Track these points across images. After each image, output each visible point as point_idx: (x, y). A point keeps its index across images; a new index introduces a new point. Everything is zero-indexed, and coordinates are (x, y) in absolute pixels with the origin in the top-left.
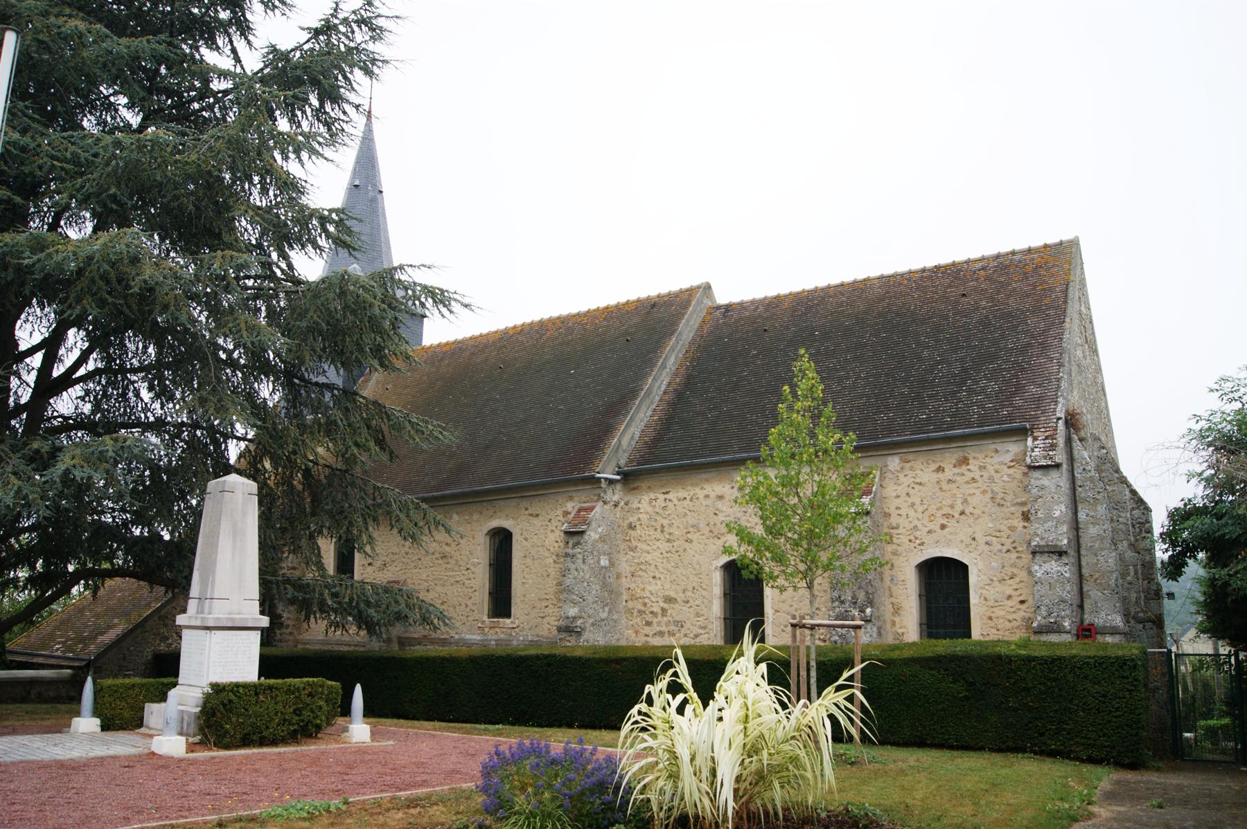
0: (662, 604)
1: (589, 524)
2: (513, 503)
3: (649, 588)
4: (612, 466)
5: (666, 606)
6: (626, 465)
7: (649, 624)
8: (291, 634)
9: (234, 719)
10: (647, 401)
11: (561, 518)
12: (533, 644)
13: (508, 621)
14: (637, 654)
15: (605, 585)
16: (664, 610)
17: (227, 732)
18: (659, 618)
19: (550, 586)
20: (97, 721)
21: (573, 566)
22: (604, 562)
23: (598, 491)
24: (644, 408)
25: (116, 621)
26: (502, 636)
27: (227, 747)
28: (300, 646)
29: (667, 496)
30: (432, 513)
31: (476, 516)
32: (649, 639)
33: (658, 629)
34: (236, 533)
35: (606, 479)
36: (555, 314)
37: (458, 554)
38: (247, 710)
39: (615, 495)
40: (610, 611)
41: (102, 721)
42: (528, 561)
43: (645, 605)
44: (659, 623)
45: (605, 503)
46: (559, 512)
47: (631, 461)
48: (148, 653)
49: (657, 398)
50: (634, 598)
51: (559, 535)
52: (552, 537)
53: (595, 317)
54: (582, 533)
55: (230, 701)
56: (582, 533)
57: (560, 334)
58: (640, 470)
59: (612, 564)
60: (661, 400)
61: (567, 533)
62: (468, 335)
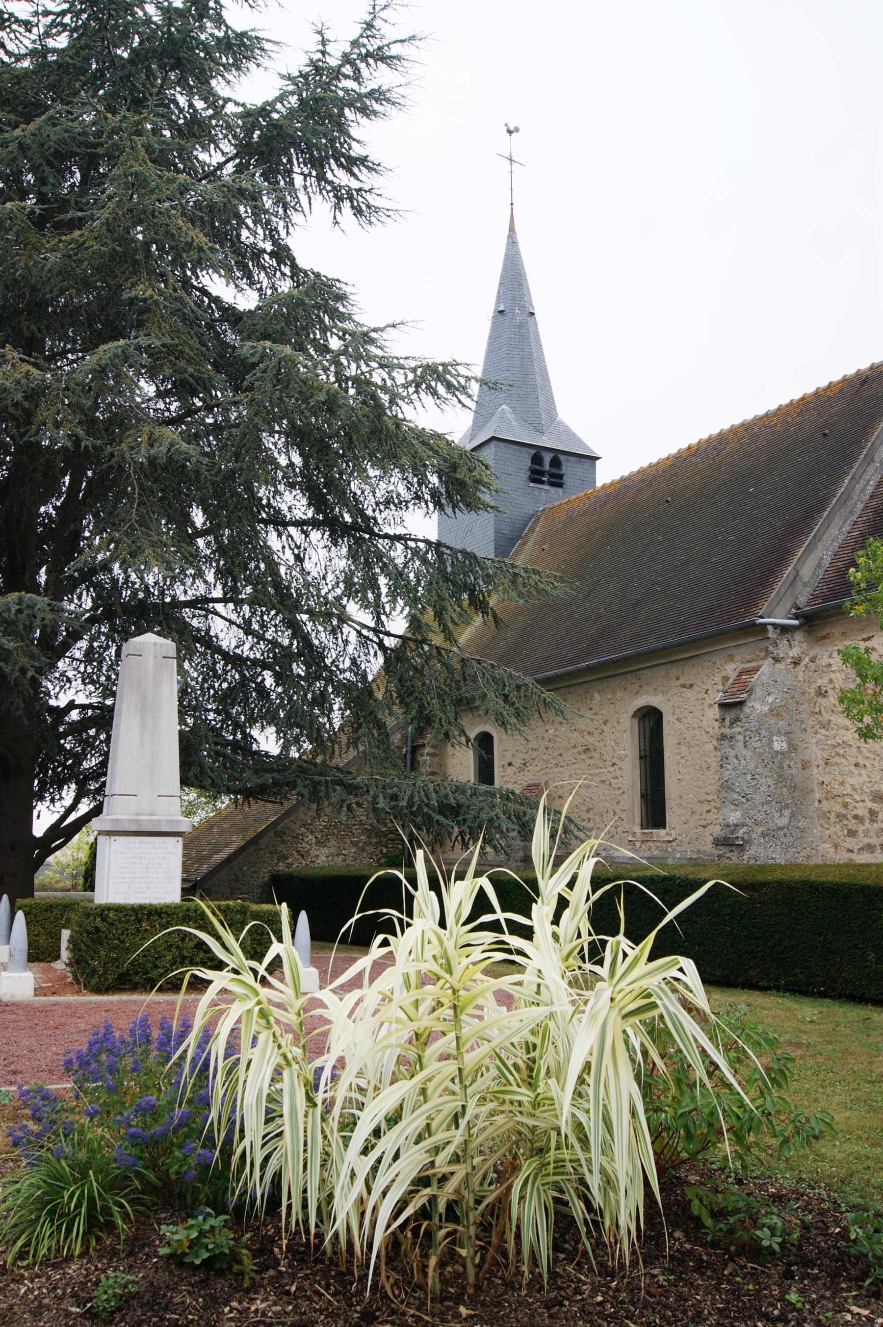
0: (870, 804)
1: (750, 692)
2: (661, 672)
3: (850, 780)
4: (787, 604)
5: (875, 807)
6: (808, 604)
7: (852, 833)
9: (103, 953)
10: (844, 512)
13: (662, 832)
14: (778, 876)
15: (781, 778)
16: (872, 812)
17: (94, 971)
18: (867, 825)
19: (711, 781)
21: (732, 753)
22: (779, 744)
23: (765, 644)
24: (837, 522)
27: (98, 991)
29: (869, 644)
30: (548, 695)
31: (619, 694)
32: (854, 856)
33: (866, 841)
34: (146, 708)
35: (775, 625)
37: (602, 744)
38: (123, 942)
39: (797, 646)
40: (793, 815)
43: (846, 805)
44: (867, 833)
45: (777, 660)
46: (718, 679)
47: (815, 597)
48: (264, 875)
49: (860, 506)
50: (830, 796)
51: (715, 712)
53: (787, 414)
54: (741, 704)
55: (97, 929)
56: (741, 704)
57: (742, 445)
58: (827, 610)
59: (793, 747)
60: (866, 508)
61: (724, 706)
62: (635, 469)
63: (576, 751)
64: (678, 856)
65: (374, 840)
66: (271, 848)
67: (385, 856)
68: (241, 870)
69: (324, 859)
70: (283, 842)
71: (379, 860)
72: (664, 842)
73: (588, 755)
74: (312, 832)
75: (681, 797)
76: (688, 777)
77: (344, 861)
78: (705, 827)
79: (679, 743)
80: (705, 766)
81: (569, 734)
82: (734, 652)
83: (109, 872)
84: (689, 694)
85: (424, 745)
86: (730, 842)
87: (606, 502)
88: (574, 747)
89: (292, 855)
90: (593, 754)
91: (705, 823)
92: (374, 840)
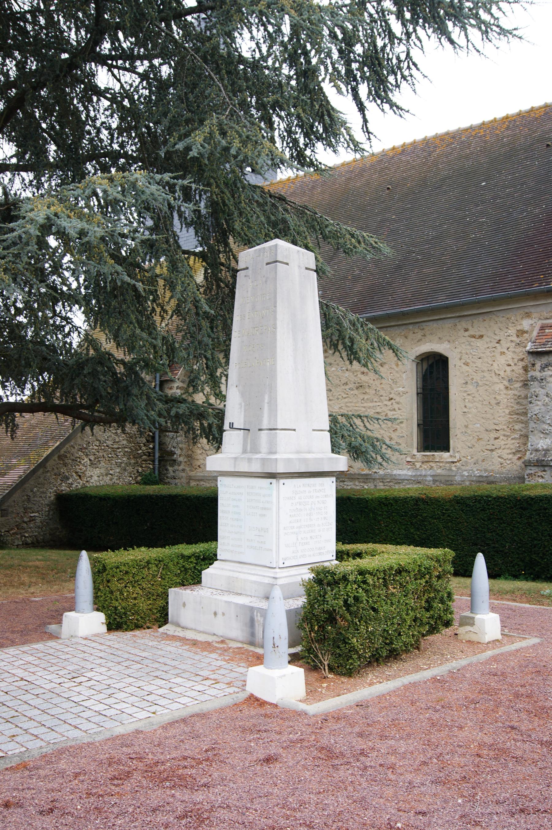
2: (448, 324)
8: (183, 470)
11: (514, 338)
12: (480, 480)
13: (445, 455)
20: (101, 617)
25: (14, 461)
26: (439, 471)
28: (193, 484)
36: (441, 130)
41: (108, 617)
42: (471, 388)
46: (512, 331)
52: (502, 360)
57: (454, 149)
63: (347, 387)
64: (466, 473)
65: (133, 461)
66: (56, 471)
67: (140, 474)
68: (32, 491)
69: (96, 478)
70: (65, 465)
71: (136, 477)
72: (447, 462)
73: (361, 390)
74: (87, 455)
75: (466, 427)
76: (474, 411)
77: (111, 480)
78: (492, 450)
79: (466, 383)
80: (493, 402)
81: (340, 373)
82: (532, 310)
83: (278, 523)
84: (479, 343)
85: (172, 381)
86: (544, 463)
87: (313, 187)
88: (346, 384)
89: (72, 476)
90: (368, 391)
91: (493, 448)
92: (133, 461)
